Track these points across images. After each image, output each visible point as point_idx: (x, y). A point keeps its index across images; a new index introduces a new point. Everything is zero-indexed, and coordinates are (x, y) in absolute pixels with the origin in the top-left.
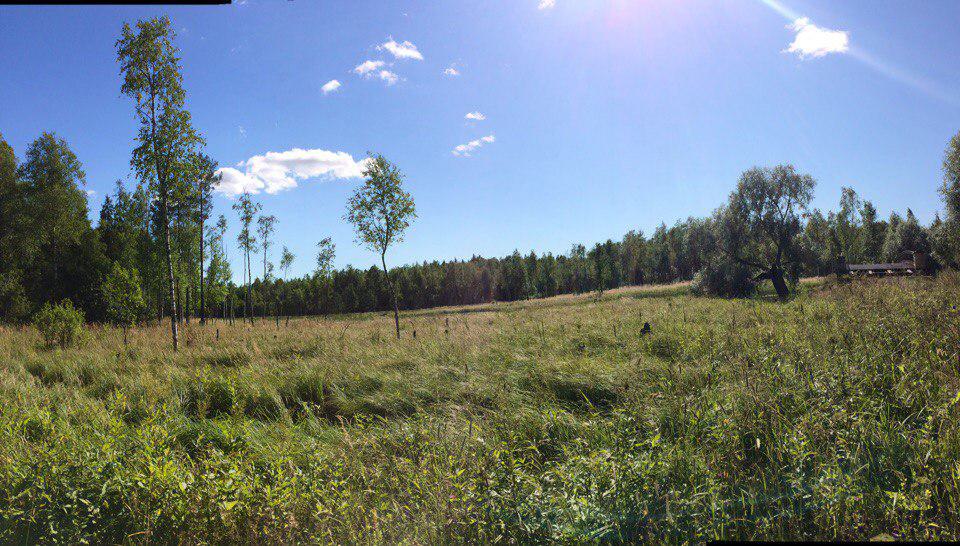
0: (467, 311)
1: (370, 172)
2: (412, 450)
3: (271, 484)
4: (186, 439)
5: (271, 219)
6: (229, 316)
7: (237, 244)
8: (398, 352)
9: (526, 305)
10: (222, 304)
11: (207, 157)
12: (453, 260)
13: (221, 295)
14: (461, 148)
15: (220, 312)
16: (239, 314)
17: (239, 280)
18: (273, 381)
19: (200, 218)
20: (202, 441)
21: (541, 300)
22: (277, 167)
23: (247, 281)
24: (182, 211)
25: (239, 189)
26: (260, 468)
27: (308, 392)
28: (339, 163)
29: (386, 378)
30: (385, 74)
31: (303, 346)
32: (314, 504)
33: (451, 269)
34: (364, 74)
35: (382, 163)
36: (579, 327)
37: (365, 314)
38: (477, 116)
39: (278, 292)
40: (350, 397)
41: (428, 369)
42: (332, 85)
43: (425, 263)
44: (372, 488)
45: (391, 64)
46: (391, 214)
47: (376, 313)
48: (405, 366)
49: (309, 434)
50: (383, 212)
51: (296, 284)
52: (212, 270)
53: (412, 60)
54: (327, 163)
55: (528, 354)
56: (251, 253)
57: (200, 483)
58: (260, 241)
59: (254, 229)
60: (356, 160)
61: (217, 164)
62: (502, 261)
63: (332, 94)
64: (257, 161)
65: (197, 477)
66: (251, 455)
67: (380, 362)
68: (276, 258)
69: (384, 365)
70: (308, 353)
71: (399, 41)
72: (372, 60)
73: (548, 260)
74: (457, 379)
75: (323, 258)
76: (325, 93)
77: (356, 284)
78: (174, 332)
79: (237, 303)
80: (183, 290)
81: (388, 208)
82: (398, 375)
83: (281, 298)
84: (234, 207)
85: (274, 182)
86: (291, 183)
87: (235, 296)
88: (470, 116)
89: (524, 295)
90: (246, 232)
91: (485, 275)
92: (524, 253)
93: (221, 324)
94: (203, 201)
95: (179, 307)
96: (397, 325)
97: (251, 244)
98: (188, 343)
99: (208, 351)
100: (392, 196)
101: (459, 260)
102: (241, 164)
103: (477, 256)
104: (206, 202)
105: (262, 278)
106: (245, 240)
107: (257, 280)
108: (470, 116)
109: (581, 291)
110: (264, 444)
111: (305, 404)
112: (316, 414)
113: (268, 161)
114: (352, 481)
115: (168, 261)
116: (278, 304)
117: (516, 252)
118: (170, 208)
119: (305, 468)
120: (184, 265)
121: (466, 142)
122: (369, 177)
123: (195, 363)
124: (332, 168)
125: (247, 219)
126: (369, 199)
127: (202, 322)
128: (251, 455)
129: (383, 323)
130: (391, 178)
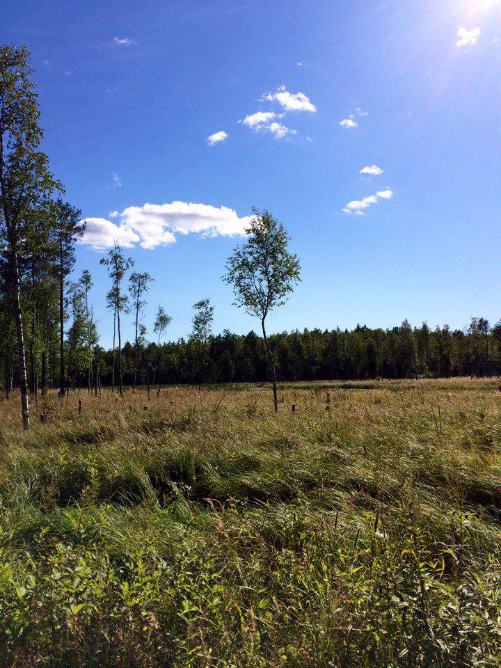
0: (349, 387)
1: (253, 230)
2: (292, 540)
3: (130, 581)
4: (27, 535)
5: (145, 276)
6: (94, 385)
7: (105, 303)
8: (278, 427)
9: (414, 385)
10: (87, 371)
11: (67, 204)
12: (336, 329)
13: (85, 360)
14: (354, 204)
15: (83, 381)
16: (107, 382)
17: (107, 343)
18: (140, 458)
19: (60, 272)
20: (45, 536)
21: (433, 380)
22: (154, 220)
23: (117, 345)
24: (36, 264)
25: (110, 243)
26: (118, 560)
27: (178, 471)
28: (220, 219)
29: (263, 457)
30: (275, 126)
31: (177, 418)
32: (179, 599)
33: (334, 338)
34: (254, 125)
35: (267, 222)
36: (482, 416)
37: (241, 385)
38: (374, 170)
39: (150, 357)
40: (223, 476)
41: (309, 453)
42: (219, 136)
43: (306, 330)
44: (250, 583)
45: (281, 116)
46: (273, 276)
47: (253, 385)
48: (282, 444)
49: (177, 520)
50: (265, 273)
51: (170, 348)
52: (75, 332)
53: (304, 113)
54: (209, 218)
55: (422, 441)
56: (122, 313)
57: (42, 586)
58: (132, 300)
59: (125, 286)
60: (240, 215)
61: (79, 212)
62: (389, 332)
63: (219, 143)
64: (133, 213)
65: (39, 580)
66: (107, 547)
67: (258, 438)
68: (149, 320)
69: (261, 441)
70: (182, 426)
71: (293, 91)
72: (263, 112)
73: (443, 335)
74: (343, 462)
75: (200, 322)
76: (213, 144)
77: (232, 352)
78: (24, 406)
79: (104, 369)
80: (38, 356)
81: (270, 269)
82: (277, 455)
83: (154, 364)
84: (102, 261)
85: (150, 235)
86: (169, 238)
87: (102, 361)
88: (366, 170)
89: (412, 374)
90: (117, 290)
91: (370, 348)
92: (415, 324)
93: (85, 394)
94: (63, 254)
95: (31, 369)
96: (275, 398)
97: (121, 303)
98: (42, 419)
99: (69, 427)
100: (275, 257)
101: (343, 330)
102: (115, 214)
103: (362, 325)
104: (67, 255)
105: (132, 342)
106: (115, 298)
107: (128, 344)
108: (366, 170)
109: (480, 375)
110: (125, 533)
111: (174, 484)
112: (186, 497)
113: (145, 214)
114: (226, 575)
115: (18, 322)
116: (151, 372)
117: (405, 323)
118: (21, 260)
119: (170, 560)
120: (40, 327)
121: (360, 198)
122: (252, 235)
123: (50, 442)
124: (213, 224)
125: (118, 276)
126: (250, 259)
127: (62, 394)
128: (107, 547)
129: (259, 395)
130: (276, 239)
